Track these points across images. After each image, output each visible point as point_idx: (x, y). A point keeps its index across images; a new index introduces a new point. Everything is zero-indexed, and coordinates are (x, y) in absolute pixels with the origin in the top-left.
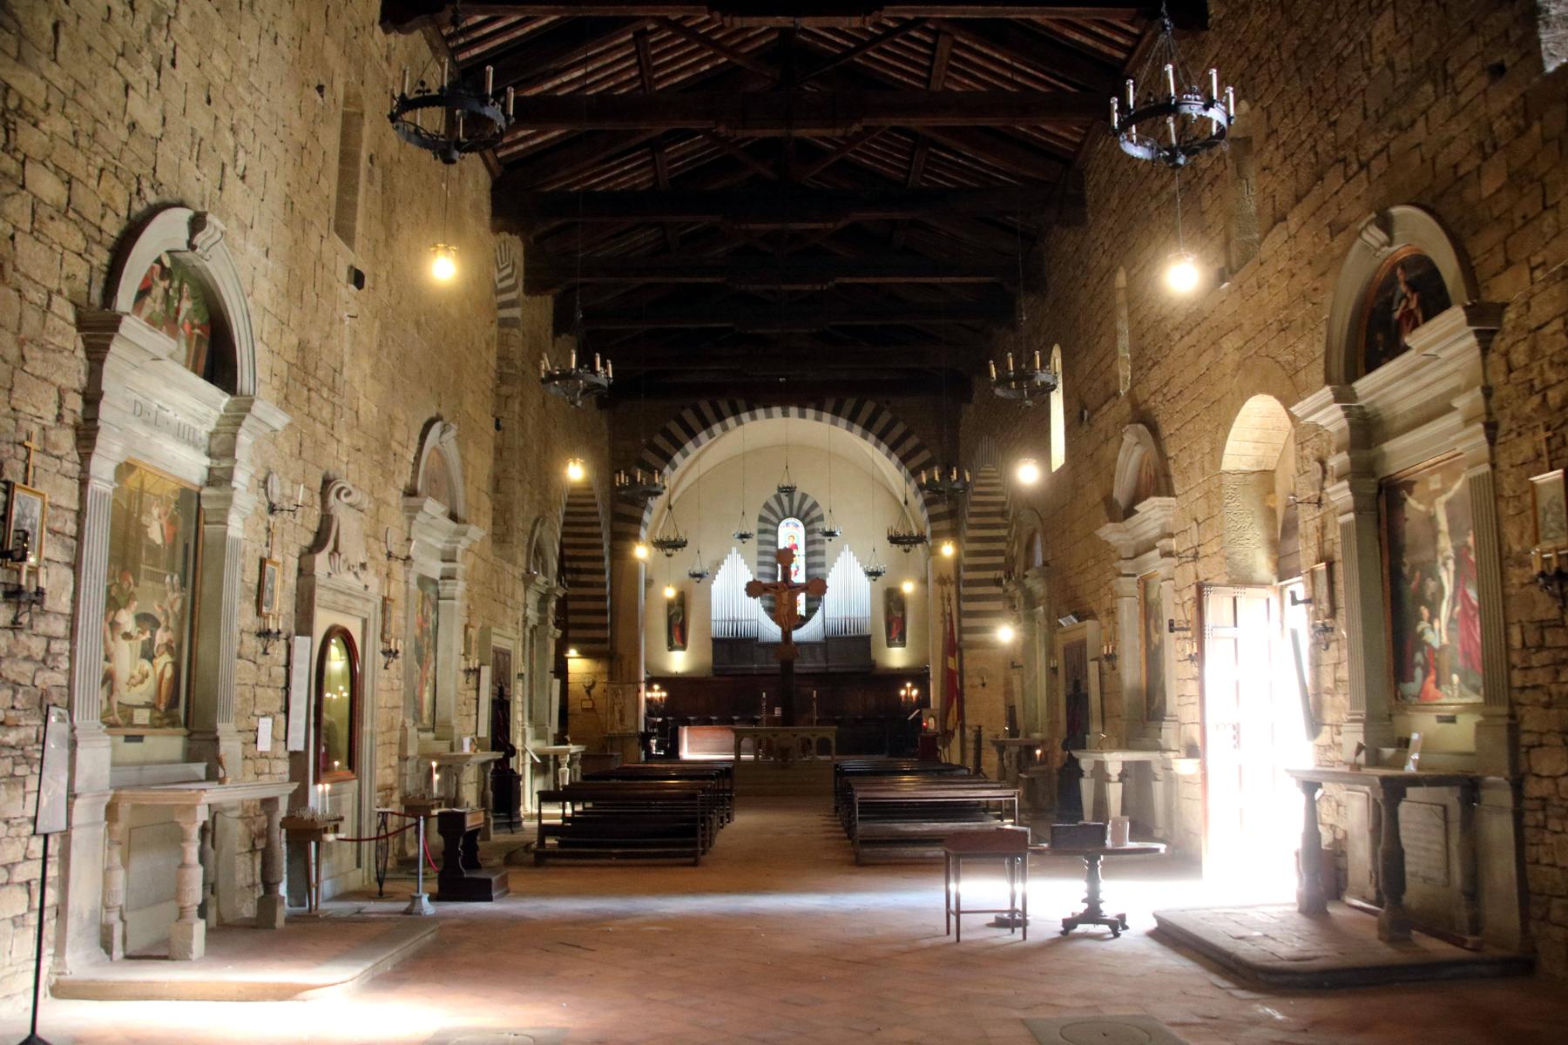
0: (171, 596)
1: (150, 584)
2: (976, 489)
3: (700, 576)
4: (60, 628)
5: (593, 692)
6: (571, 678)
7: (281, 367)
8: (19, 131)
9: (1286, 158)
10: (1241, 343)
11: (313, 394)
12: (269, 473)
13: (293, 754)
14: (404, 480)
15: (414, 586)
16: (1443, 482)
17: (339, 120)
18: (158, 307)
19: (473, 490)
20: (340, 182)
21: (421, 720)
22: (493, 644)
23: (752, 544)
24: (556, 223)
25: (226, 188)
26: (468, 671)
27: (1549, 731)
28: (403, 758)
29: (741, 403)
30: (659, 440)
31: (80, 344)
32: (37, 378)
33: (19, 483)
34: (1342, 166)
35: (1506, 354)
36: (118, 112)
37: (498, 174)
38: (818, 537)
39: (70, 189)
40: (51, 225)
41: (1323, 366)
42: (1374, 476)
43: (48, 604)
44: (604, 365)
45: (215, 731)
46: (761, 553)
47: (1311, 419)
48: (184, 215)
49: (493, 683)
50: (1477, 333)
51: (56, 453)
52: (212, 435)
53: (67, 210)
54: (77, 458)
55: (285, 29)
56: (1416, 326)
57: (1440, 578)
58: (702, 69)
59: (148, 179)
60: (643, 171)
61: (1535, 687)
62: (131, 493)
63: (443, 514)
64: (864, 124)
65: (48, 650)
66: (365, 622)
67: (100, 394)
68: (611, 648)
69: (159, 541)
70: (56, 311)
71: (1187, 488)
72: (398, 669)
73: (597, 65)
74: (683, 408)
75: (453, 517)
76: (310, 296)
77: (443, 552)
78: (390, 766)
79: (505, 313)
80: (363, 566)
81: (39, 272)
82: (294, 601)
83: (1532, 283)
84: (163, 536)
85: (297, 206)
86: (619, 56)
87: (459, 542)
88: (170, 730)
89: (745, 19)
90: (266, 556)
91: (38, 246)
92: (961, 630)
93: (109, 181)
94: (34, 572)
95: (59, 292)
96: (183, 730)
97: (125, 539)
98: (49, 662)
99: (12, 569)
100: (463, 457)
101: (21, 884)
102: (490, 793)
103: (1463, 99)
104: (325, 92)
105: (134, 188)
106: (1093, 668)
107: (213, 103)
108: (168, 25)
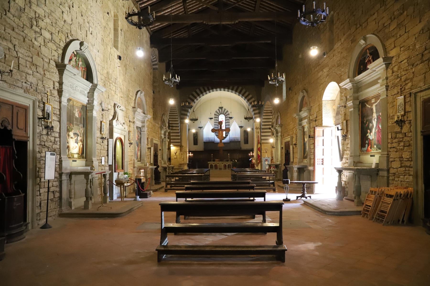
0: (81, 129)
1: (76, 126)
2: (265, 107)
4: (57, 135)
5: (176, 154)
6: (171, 151)
8: (39, 22)
9: (342, 25)
11: (111, 84)
13: (109, 165)
14: (133, 105)
15: (135, 128)
16: (375, 100)
17: (113, 21)
18: (74, 63)
19: (148, 107)
21: (138, 159)
25: (88, 36)
26: (148, 148)
27: (396, 158)
28: (134, 167)
29: (210, 88)
30: (191, 96)
31: (57, 71)
32: (48, 79)
33: (46, 102)
35: (392, 69)
36: (61, 18)
37: (151, 34)
38: (229, 118)
39: (52, 36)
40: (48, 44)
42: (358, 100)
43: (54, 130)
44: (178, 77)
45: (92, 159)
46: (215, 122)
47: (344, 87)
48: (78, 42)
49: (154, 151)
50: (385, 64)
51: (54, 96)
52: (88, 93)
53: (52, 40)
54: (58, 97)
56: (371, 63)
57: (373, 123)
58: (199, 9)
59: (70, 34)
60: (186, 33)
61: (394, 147)
62: (71, 106)
64: (239, 21)
65: (55, 140)
66: (125, 136)
67: (63, 83)
68: (181, 144)
69: (78, 117)
70: (51, 64)
71: (314, 105)
72: (133, 147)
73: (174, 8)
74: (196, 89)
75: (144, 113)
76: (109, 62)
77: (142, 121)
78: (131, 169)
79: (155, 67)
80: (124, 123)
81: (47, 54)
83: (400, 51)
84: (78, 116)
85: (105, 41)
86: (179, 6)
90: (102, 121)
91: (46, 49)
92: (261, 140)
93: (60, 34)
94: (51, 122)
95: (52, 59)
96: (85, 160)
97: (70, 116)
98: (55, 143)
99: (46, 122)
100: (146, 99)
101: (52, 192)
102: (154, 175)
103: (387, 7)
104: (109, 14)
105: (66, 36)
106: (291, 147)
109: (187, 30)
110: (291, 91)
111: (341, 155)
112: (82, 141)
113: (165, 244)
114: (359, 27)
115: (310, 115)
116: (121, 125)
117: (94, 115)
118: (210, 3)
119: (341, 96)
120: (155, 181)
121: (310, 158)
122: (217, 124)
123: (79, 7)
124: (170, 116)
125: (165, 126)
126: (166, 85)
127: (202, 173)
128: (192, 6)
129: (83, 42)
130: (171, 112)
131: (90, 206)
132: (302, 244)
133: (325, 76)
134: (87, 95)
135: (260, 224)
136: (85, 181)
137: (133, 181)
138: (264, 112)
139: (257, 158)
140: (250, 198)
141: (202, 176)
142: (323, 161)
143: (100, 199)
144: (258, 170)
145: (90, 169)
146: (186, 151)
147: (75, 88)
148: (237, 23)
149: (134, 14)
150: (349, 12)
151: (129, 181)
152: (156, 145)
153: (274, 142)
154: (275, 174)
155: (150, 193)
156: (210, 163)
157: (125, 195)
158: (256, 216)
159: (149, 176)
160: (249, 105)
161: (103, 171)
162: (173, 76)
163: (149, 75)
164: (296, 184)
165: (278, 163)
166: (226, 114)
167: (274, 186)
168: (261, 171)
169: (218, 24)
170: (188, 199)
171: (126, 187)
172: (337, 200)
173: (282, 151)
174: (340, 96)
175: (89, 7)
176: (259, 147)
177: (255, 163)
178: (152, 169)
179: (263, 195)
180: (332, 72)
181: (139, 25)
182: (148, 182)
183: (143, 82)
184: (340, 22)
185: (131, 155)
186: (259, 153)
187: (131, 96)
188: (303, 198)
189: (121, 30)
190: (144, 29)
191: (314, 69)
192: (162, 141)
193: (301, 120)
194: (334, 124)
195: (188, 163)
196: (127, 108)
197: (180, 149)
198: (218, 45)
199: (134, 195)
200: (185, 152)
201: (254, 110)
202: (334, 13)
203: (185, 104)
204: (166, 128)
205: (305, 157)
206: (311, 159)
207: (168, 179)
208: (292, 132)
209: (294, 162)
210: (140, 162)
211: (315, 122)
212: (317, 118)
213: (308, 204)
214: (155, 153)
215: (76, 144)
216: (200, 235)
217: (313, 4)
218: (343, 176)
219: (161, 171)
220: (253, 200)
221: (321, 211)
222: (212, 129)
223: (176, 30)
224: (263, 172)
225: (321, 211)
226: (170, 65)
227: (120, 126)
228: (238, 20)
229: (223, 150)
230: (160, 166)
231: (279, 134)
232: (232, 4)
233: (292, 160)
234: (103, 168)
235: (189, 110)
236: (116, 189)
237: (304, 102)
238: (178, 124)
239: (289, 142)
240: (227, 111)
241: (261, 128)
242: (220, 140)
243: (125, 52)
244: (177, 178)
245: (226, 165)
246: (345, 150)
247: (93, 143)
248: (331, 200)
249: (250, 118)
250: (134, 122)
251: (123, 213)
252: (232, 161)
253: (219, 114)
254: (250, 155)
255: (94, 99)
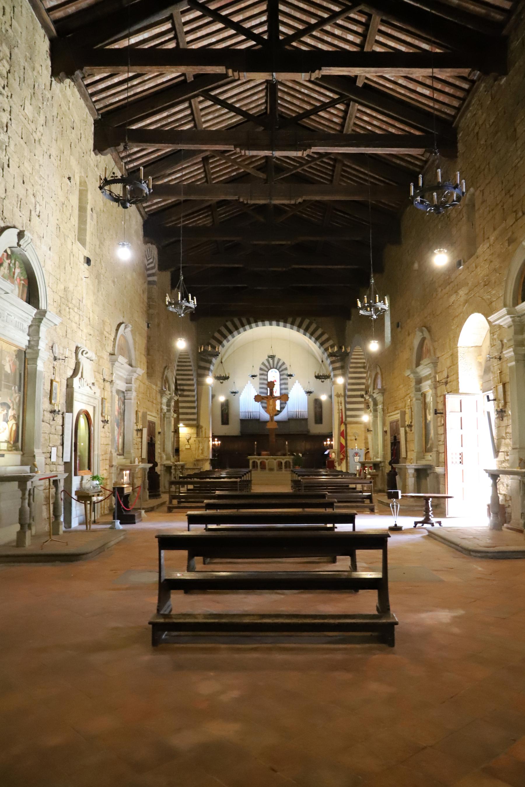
1: (6, 390)
2: (353, 357)
3: (235, 393)
5: (190, 441)
7: (57, 298)
9: (490, 212)
10: (467, 292)
11: (71, 310)
12: (54, 344)
13: (66, 463)
14: (110, 349)
15: (114, 393)
17: (77, 193)
18: (6, 271)
20: (79, 220)
21: (118, 451)
22: (148, 419)
23: (257, 379)
24: (172, 240)
25: (32, 220)
26: (138, 430)
28: (111, 466)
29: (252, 319)
30: (217, 335)
34: (514, 214)
37: (146, 218)
41: (503, 301)
44: (192, 299)
45: (34, 452)
46: (261, 384)
47: (497, 322)
48: (15, 232)
49: (148, 435)
52: (30, 327)
55: (54, 152)
63: (126, 363)
66: (94, 407)
68: (198, 423)
69: (9, 372)
71: (443, 354)
72: (108, 428)
73: (187, 171)
74: (227, 321)
75: (131, 365)
76: (68, 268)
77: (126, 379)
78: (106, 469)
79: (151, 279)
80: (93, 384)
82: (65, 398)
85: (62, 229)
86: (196, 168)
87: (133, 375)
88: (15, 452)
89: (250, 151)
96: (21, 453)
100: (134, 339)
102: (147, 481)
104: (72, 180)
106: (402, 431)
107: (25, 184)
108: (6, 149)
109: (210, 213)
110: (399, 329)
111: (496, 447)
112: (16, 418)
113: (165, 611)
114: (520, 217)
115: (436, 373)
116: (88, 387)
117: (38, 368)
118: (251, 166)
119: (492, 339)
120: (149, 493)
121: (437, 451)
122: (265, 386)
123: (19, 167)
124: (178, 370)
125: (169, 390)
126: (172, 312)
127: (236, 478)
128: (218, 169)
129: (23, 231)
130: (180, 364)
131: (28, 541)
132: (427, 611)
133: (462, 304)
134: (27, 330)
135: (346, 573)
136: (20, 493)
137: (108, 493)
138: (351, 365)
139: (339, 450)
140: (326, 523)
141: (236, 482)
142: (462, 456)
143: (46, 528)
144: (341, 471)
145: (29, 470)
146: (207, 436)
147: (5, 318)
148: (300, 203)
149: (115, 181)
150: (502, 190)
151: (101, 492)
152: (151, 424)
153: (370, 420)
154: (372, 481)
155: (140, 514)
156: (252, 458)
157: (93, 519)
158: (338, 557)
159: (138, 482)
160: (323, 353)
161: (54, 473)
162: (185, 297)
163: (140, 295)
164: (412, 499)
165: (379, 460)
166: (281, 368)
167: (371, 502)
168: (347, 473)
169: (265, 204)
170: (210, 526)
171: (96, 504)
172: (491, 529)
173: (386, 437)
174: (490, 340)
175: (37, 167)
176: (343, 430)
177: (336, 459)
178: (144, 469)
179: (350, 519)
180: (474, 295)
181: (123, 201)
182: (136, 494)
183: (129, 307)
184: (486, 208)
185: (105, 443)
186: (343, 441)
187: (108, 333)
188: (426, 525)
189: (92, 209)
190: (132, 208)
191: (442, 290)
192: (163, 417)
193: (419, 381)
194: (481, 390)
195: (211, 457)
196: (100, 355)
197: (195, 432)
198: (266, 243)
199: (110, 518)
200: (206, 437)
201: (332, 362)
202: (476, 191)
203: (205, 348)
204: (170, 393)
205: (427, 450)
206: (439, 453)
207: (173, 488)
208: (404, 404)
209: (408, 457)
210: (122, 457)
211: (446, 386)
212: (449, 379)
213: (436, 537)
214: (150, 439)
215: (5, 423)
216: (234, 593)
217: (436, 174)
218: (501, 486)
219: (161, 473)
220: (333, 529)
221: (460, 549)
222: (256, 396)
223: (190, 211)
224: (350, 477)
225: (460, 549)
226: (179, 276)
227: (86, 390)
228: (302, 198)
229: (277, 435)
230: (159, 464)
231: (380, 407)
232: (292, 168)
233: (403, 454)
234: (53, 467)
235: (214, 360)
236: (78, 508)
237: (424, 348)
238: (193, 385)
239: (398, 421)
240: (284, 364)
241: (345, 395)
242: (270, 417)
243: (98, 250)
244: (191, 487)
245: (281, 463)
246: (503, 438)
247: (36, 423)
248: (480, 528)
249: (325, 376)
250: (112, 381)
251: (87, 553)
252: (294, 455)
253: (269, 367)
254: (327, 444)
255: (39, 338)
